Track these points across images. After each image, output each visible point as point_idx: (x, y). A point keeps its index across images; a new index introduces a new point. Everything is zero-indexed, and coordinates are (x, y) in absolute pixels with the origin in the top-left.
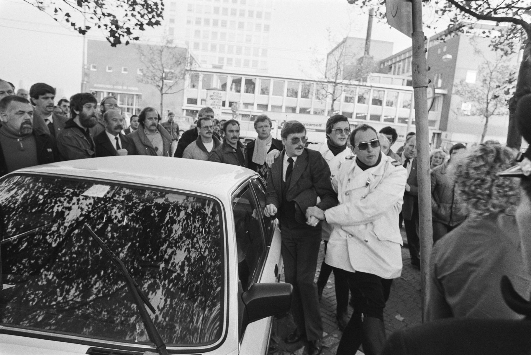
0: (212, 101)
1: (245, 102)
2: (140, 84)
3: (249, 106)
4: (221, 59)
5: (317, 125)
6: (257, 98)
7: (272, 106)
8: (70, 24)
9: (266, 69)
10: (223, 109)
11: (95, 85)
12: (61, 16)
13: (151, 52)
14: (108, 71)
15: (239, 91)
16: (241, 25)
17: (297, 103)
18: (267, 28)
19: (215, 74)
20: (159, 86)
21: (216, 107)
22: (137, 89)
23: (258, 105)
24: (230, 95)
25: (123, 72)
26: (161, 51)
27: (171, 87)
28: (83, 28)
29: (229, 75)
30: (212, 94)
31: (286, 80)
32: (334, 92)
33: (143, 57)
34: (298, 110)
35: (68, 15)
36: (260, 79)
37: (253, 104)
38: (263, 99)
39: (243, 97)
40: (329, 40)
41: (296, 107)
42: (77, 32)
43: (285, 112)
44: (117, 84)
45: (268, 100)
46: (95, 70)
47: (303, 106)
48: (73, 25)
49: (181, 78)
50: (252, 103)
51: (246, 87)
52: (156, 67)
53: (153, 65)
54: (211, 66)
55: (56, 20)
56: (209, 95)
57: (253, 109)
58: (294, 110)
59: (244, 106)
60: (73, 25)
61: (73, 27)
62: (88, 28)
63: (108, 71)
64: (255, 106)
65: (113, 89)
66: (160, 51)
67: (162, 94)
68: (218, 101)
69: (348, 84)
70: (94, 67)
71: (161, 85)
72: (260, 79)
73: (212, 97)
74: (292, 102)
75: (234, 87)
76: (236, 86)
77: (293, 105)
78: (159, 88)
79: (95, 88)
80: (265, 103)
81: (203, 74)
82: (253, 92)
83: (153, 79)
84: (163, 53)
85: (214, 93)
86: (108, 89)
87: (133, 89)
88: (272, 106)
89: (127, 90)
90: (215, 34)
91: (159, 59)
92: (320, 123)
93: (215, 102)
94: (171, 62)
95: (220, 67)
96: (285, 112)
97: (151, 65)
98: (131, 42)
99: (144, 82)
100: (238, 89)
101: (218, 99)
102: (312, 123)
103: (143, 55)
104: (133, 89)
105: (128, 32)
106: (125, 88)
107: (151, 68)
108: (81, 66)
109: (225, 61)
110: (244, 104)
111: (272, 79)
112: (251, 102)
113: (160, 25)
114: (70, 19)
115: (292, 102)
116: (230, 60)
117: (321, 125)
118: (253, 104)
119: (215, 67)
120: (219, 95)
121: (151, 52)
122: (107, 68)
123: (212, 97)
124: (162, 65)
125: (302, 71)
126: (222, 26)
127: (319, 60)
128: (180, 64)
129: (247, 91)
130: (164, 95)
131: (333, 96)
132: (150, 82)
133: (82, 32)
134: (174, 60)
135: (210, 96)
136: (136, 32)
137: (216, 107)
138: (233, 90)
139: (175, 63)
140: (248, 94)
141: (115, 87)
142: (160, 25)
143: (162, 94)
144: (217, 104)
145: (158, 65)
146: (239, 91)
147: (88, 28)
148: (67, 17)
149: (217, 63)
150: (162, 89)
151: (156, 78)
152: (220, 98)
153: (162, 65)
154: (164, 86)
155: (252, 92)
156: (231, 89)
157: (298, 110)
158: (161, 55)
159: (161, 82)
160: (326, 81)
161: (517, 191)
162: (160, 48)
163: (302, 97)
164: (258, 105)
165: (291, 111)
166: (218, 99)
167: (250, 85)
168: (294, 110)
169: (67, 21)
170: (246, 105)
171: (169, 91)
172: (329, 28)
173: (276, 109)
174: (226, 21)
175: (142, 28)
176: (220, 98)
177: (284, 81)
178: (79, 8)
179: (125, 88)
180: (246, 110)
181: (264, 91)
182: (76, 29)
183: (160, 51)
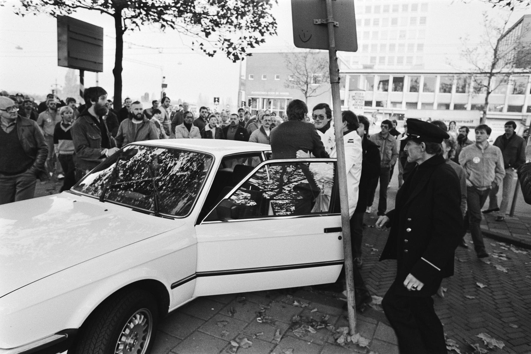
0: (354, 101)
1: (393, 101)
2: (288, 89)
3: (398, 105)
4: (373, 59)
5: (468, 122)
6: (406, 95)
7: (423, 104)
8: (203, 50)
9: (421, 65)
10: (365, 109)
11: (252, 93)
12: (197, 46)
13: (296, 59)
14: (263, 79)
15: (386, 90)
16: (394, 22)
17: (451, 99)
18: (423, 20)
19: (361, 75)
20: (304, 90)
21: (358, 107)
22: (287, 94)
23: (407, 103)
24: (377, 95)
25: (276, 79)
26: (305, 57)
27: (315, 90)
28: (212, 53)
29: (376, 75)
30: (354, 95)
31: (438, 75)
32: (489, 84)
33: (290, 65)
34: (452, 107)
35: (202, 44)
36: (378, 76)
37: (401, 103)
38: (412, 97)
39: (392, 95)
40: (485, 25)
41: (450, 103)
42: (208, 55)
43: (421, 109)
44: (271, 90)
45: (418, 98)
46: (252, 79)
47: (459, 102)
48: (205, 51)
49: (324, 81)
50: (400, 101)
51: (395, 85)
52: (301, 73)
53: (299, 71)
54: (362, 67)
55: (193, 49)
56: (351, 96)
57: (401, 107)
58: (447, 106)
59: (392, 105)
60: (205, 51)
61: (205, 53)
62: (215, 52)
63: (263, 79)
64: (404, 104)
65: (267, 95)
66: (304, 57)
67: (307, 98)
68: (360, 101)
69: (509, 73)
70: (252, 77)
71: (305, 88)
72: (409, 76)
73: (354, 98)
74: (445, 98)
75: (381, 86)
76: (384, 84)
77: (446, 101)
78: (304, 92)
79: (253, 95)
80: (414, 101)
81: (350, 76)
82: (402, 90)
83: (298, 83)
84: (307, 59)
85: (356, 94)
86: (263, 95)
87: (284, 94)
88: (423, 104)
89: (279, 95)
90: (376, 33)
91: (304, 65)
92: (471, 120)
93: (357, 102)
94: (316, 66)
95: (371, 67)
96: (421, 109)
97: (296, 71)
98: (245, 57)
99: (290, 87)
100: (386, 88)
101: (360, 100)
102: (460, 120)
103: (290, 63)
104: (284, 94)
105: (243, 50)
106: (277, 93)
107: (297, 74)
108: (239, 77)
109: (377, 61)
110: (392, 102)
111: (422, 75)
112: (399, 100)
113: (265, 42)
114: (203, 47)
115: (445, 98)
116: (382, 59)
117: (472, 121)
118: (401, 103)
119: (365, 67)
120: (361, 95)
121: (296, 59)
122: (262, 77)
123: (354, 98)
124: (306, 70)
125: (450, 64)
126: (374, 24)
127: (471, 50)
128: (323, 68)
129: (395, 89)
130: (308, 98)
131: (488, 88)
132: (295, 87)
133: (210, 55)
134: (318, 65)
135: (352, 97)
136: (249, 50)
137: (358, 107)
138: (381, 89)
139: (319, 67)
140: (396, 92)
141: (269, 93)
142: (265, 42)
143: (307, 98)
144: (360, 104)
145: (303, 71)
146: (386, 90)
147: (215, 52)
148: (201, 46)
149: (368, 63)
150: (306, 93)
151: (301, 83)
152: (362, 98)
153: (306, 70)
154: (309, 90)
155: (401, 90)
156: (378, 88)
157: (452, 107)
158: (306, 61)
159: (306, 86)
160: (479, 72)
161: (409, 149)
162: (304, 55)
163: (457, 91)
164: (407, 103)
165: (444, 108)
166: (360, 100)
167: (399, 82)
168: (447, 106)
169: (202, 48)
170: (394, 103)
171: (313, 94)
172: (486, 12)
173: (426, 107)
174: (379, 19)
175: (252, 47)
176: (362, 98)
177: (436, 76)
178: (206, 38)
179: (277, 93)
180: (394, 109)
181: (414, 89)
182: (207, 54)
183: (304, 57)
